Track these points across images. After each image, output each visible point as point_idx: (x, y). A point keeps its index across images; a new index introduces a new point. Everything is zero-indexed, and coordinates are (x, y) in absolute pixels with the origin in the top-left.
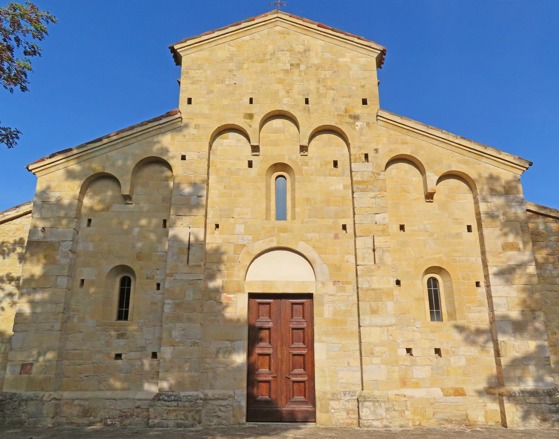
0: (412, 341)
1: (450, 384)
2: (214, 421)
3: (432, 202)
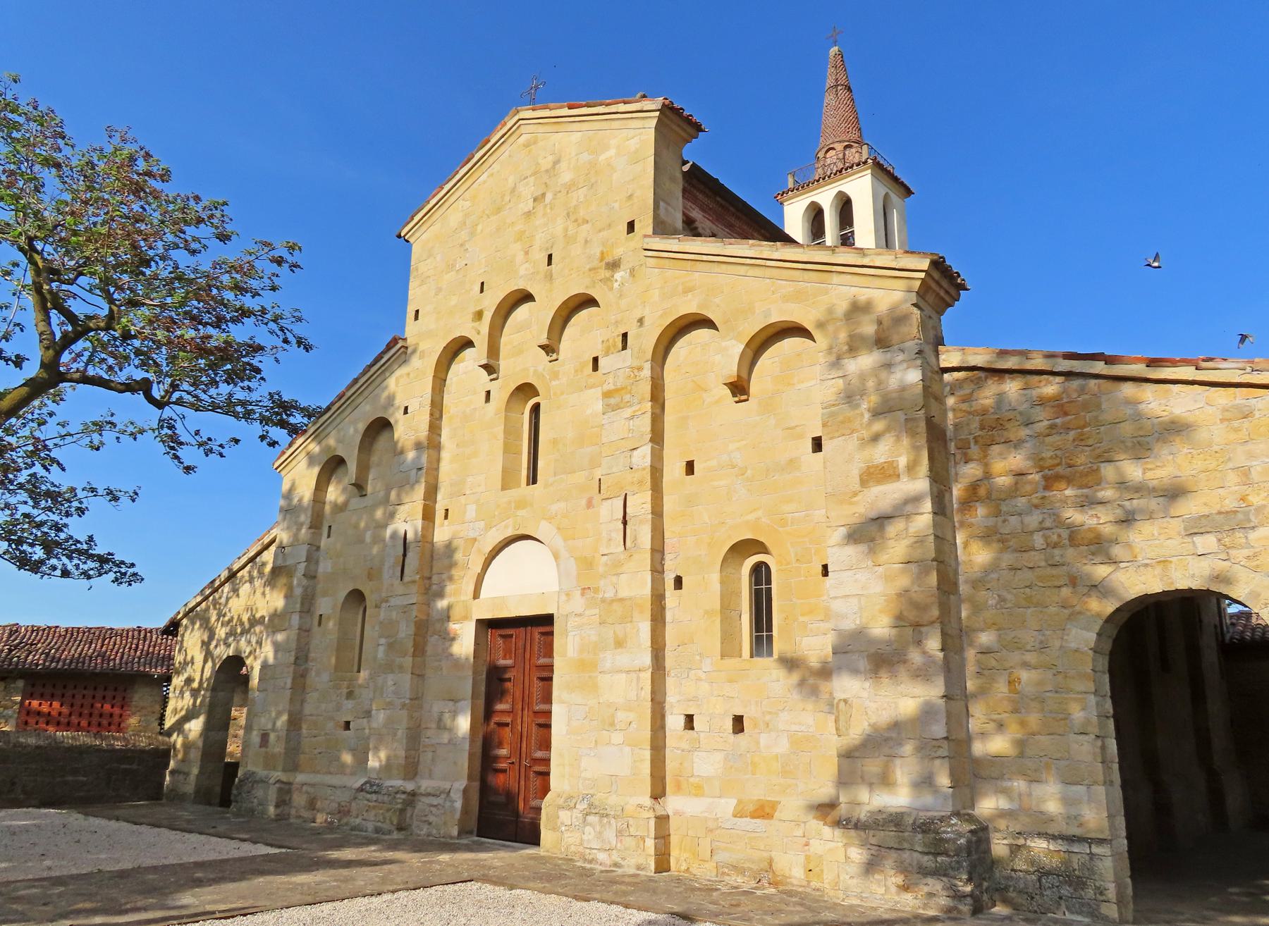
0: (695, 699)
1: (757, 793)
2: (425, 830)
3: (747, 400)
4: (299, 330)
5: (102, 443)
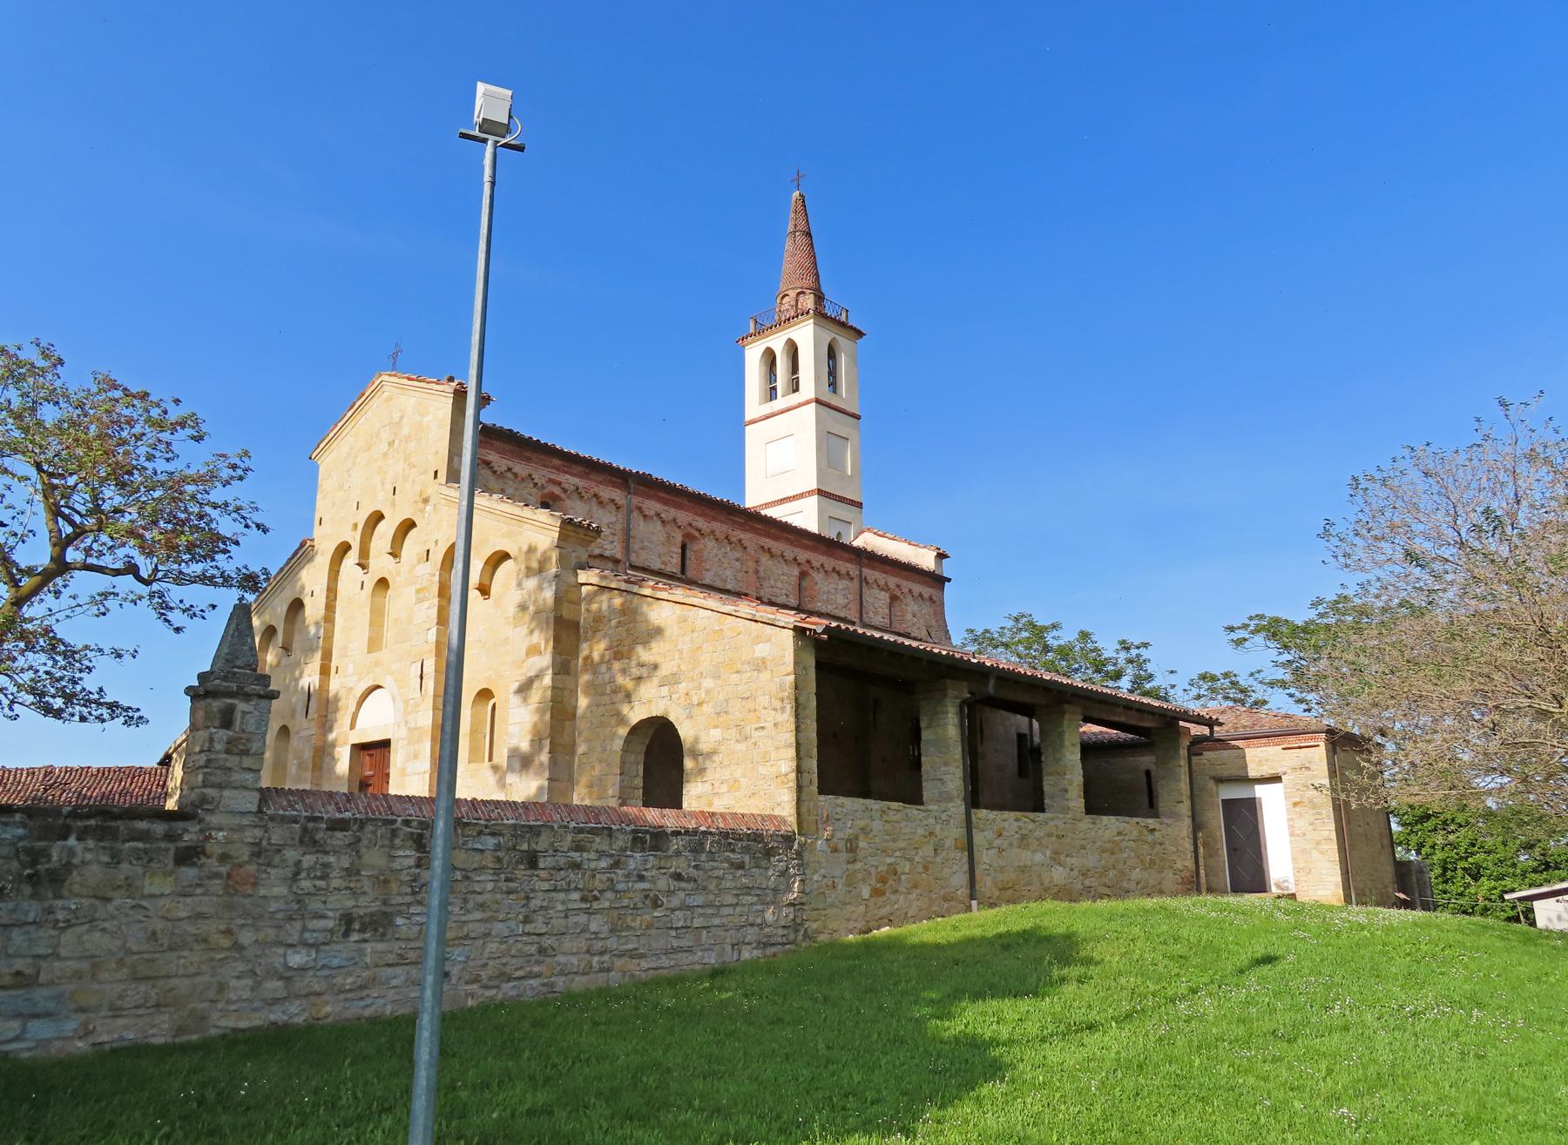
4: (257, 517)
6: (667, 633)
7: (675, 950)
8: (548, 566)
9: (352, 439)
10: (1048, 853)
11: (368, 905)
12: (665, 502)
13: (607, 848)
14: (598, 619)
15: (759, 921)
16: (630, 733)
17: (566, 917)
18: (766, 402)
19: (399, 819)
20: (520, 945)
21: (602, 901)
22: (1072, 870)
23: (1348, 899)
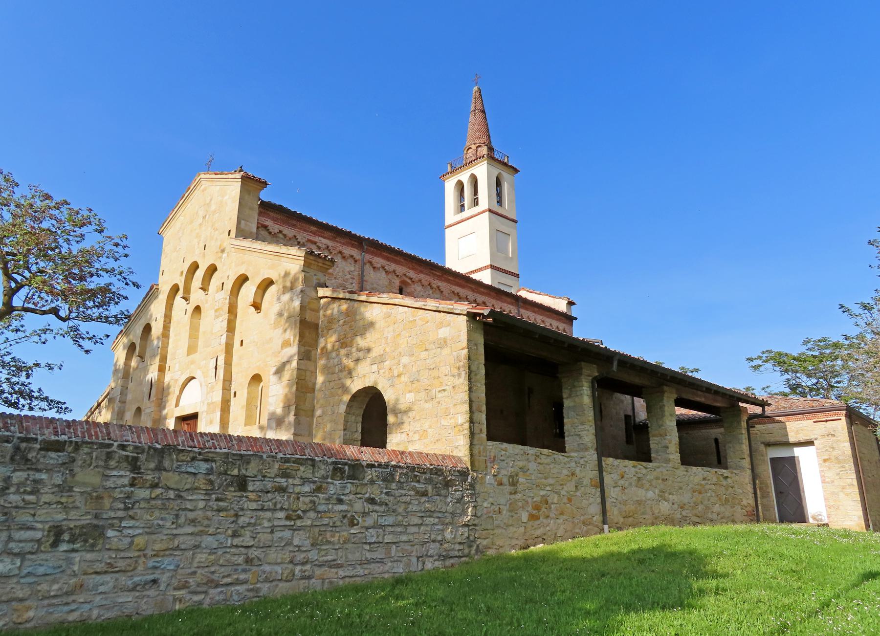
4: (133, 278)
5: (46, 340)
6: (377, 326)
7: (369, 562)
8: (297, 284)
9: (183, 218)
10: (657, 491)
11: (79, 518)
12: (388, 259)
13: (311, 476)
14: (331, 320)
15: (439, 538)
16: (350, 400)
17: (272, 532)
18: (458, 213)
19: (116, 444)
20: (228, 556)
21: (305, 519)
22: (673, 504)
23: (867, 526)
